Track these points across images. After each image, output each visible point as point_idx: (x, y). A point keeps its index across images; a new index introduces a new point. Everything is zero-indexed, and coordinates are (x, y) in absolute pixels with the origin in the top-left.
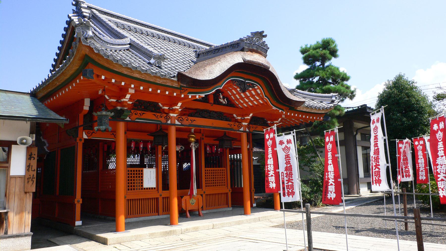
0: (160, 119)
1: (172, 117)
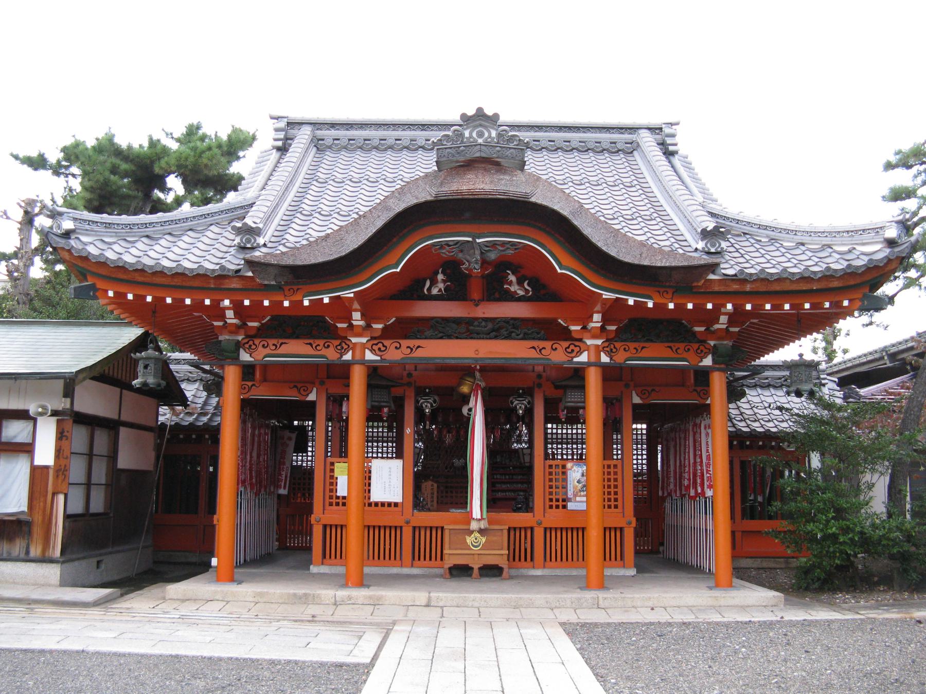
0: (324, 352)
1: (355, 344)
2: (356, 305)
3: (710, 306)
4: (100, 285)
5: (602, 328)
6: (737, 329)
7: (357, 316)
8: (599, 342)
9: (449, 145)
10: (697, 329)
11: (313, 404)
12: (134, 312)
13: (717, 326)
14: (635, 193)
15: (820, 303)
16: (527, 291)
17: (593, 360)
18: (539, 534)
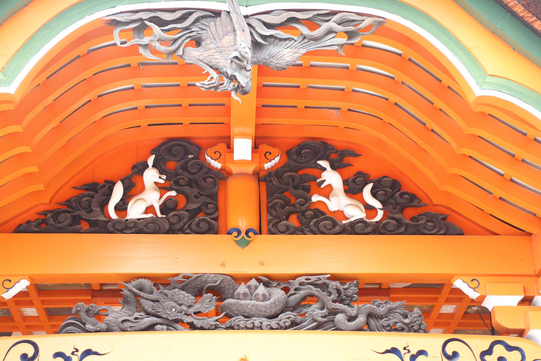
16: (369, 208)
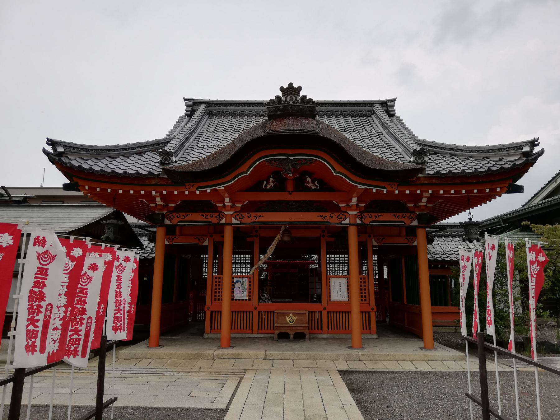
2: (227, 195)
3: (419, 192)
4: (81, 183)
5: (357, 205)
6: (431, 205)
7: (227, 200)
8: (355, 213)
9: (274, 106)
10: (409, 205)
11: (207, 247)
12: (104, 199)
13: (420, 204)
14: (373, 134)
15: (482, 190)
16: (317, 186)
17: (352, 222)
18: (325, 314)
